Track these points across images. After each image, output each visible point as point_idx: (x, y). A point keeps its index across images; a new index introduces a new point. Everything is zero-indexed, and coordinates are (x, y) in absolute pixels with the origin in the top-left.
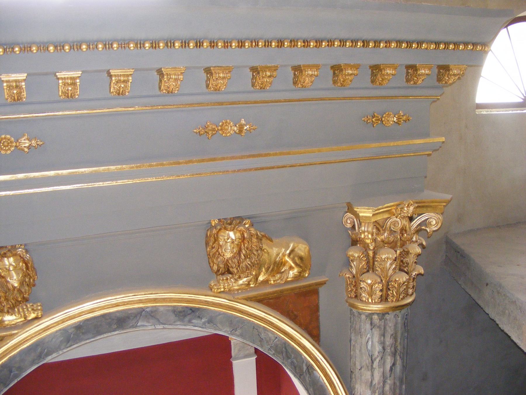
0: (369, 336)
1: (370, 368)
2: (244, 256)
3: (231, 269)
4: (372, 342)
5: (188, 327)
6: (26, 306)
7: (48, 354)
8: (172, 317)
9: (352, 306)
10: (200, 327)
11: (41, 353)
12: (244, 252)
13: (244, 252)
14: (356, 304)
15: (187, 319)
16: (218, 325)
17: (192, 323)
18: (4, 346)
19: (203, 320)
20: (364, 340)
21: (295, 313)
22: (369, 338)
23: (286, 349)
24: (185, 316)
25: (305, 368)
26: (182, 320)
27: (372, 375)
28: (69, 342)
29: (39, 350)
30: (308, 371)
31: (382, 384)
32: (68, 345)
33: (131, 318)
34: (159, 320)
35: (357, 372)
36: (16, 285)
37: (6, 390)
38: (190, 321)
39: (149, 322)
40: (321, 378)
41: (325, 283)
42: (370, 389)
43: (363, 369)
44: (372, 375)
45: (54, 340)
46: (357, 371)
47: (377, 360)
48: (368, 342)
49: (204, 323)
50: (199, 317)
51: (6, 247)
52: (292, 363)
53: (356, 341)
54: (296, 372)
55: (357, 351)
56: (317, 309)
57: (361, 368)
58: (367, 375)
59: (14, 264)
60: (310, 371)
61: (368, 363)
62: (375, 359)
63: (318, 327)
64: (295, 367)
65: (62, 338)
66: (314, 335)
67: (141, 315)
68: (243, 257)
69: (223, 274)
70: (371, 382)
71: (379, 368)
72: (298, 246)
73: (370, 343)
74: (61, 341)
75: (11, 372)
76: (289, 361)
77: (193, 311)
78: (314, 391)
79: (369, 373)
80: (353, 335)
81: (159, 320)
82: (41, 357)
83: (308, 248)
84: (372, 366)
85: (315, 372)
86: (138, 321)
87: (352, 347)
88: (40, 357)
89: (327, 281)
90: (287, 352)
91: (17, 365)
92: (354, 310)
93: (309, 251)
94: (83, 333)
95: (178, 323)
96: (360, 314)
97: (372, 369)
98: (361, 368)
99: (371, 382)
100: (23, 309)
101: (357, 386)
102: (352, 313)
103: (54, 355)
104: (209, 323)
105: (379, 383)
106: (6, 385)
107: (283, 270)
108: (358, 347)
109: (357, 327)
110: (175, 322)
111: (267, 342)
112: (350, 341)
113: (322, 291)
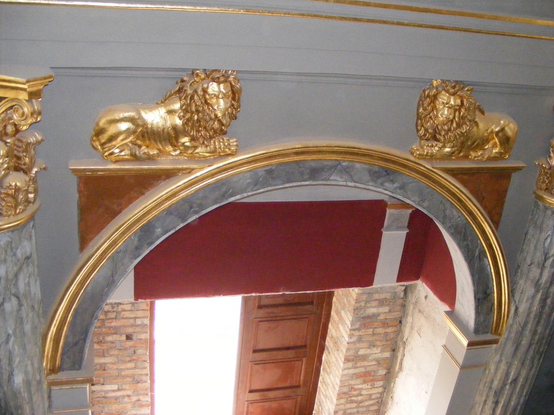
0: (549, 233)
1: (541, 266)
2: (457, 124)
3: (438, 136)
4: (551, 240)
5: (379, 190)
6: (223, 139)
7: (232, 195)
8: (367, 177)
9: (541, 198)
10: (391, 192)
11: (226, 193)
12: (457, 119)
13: (457, 119)
14: (545, 197)
15: (380, 181)
16: (409, 193)
17: (384, 186)
18: (215, 169)
19: (395, 185)
20: (543, 236)
21: (484, 194)
22: (549, 235)
23: (465, 231)
24: (379, 177)
25: (477, 253)
26: (375, 182)
27: (541, 274)
28: (256, 185)
29: (224, 189)
30: (480, 256)
31: (548, 284)
32: (255, 188)
33: (326, 170)
34: (352, 177)
35: (525, 268)
36: (220, 115)
37: (182, 225)
38: (382, 184)
39: (342, 178)
40: (488, 267)
41: (521, 169)
42: (535, 288)
43: (532, 266)
44: (541, 274)
45: (241, 181)
46: (526, 266)
47: (551, 259)
48: (546, 239)
49: (396, 188)
50: (392, 181)
51: (219, 71)
52: (468, 245)
53: (533, 236)
54: (468, 256)
55: (532, 246)
56: (506, 191)
57: (531, 264)
58: (535, 272)
59: (224, 92)
60: (481, 257)
61: (540, 260)
62: (549, 258)
63: (500, 214)
64: (468, 251)
65: (250, 180)
66: (495, 223)
67: (336, 168)
68: (454, 125)
69: (427, 140)
70: (538, 281)
71: (550, 268)
72: (508, 125)
73: (549, 240)
74: (249, 183)
75: (191, 207)
76: (465, 243)
77: (388, 174)
78: (479, 278)
79: (539, 271)
80: (531, 228)
81: (352, 177)
82: (224, 197)
83: (516, 129)
84: (543, 265)
85: (485, 259)
86: (331, 175)
87: (526, 241)
88: (224, 196)
89: (524, 167)
90: (465, 234)
91: (199, 202)
92: (539, 203)
93: (517, 133)
94: (273, 178)
95: (371, 184)
96: (546, 208)
97: (543, 267)
98: (531, 264)
99: (538, 281)
100: (220, 142)
101: (522, 282)
102: (537, 205)
103: (238, 197)
104: (400, 189)
105: (546, 283)
106: (184, 220)
107: (486, 147)
108: (534, 241)
109: (539, 222)
110: (368, 182)
111: (450, 219)
112: (526, 234)
113: (515, 177)
